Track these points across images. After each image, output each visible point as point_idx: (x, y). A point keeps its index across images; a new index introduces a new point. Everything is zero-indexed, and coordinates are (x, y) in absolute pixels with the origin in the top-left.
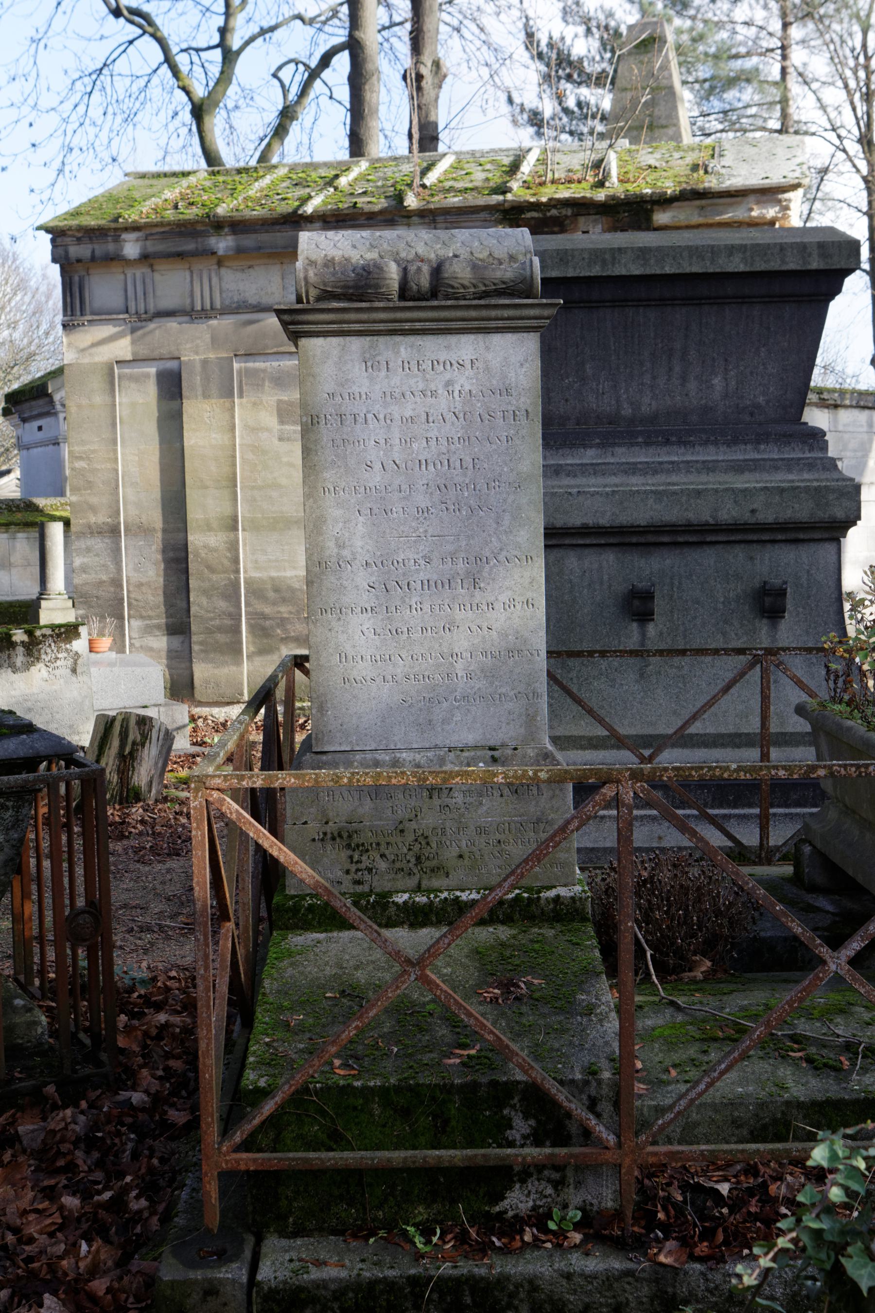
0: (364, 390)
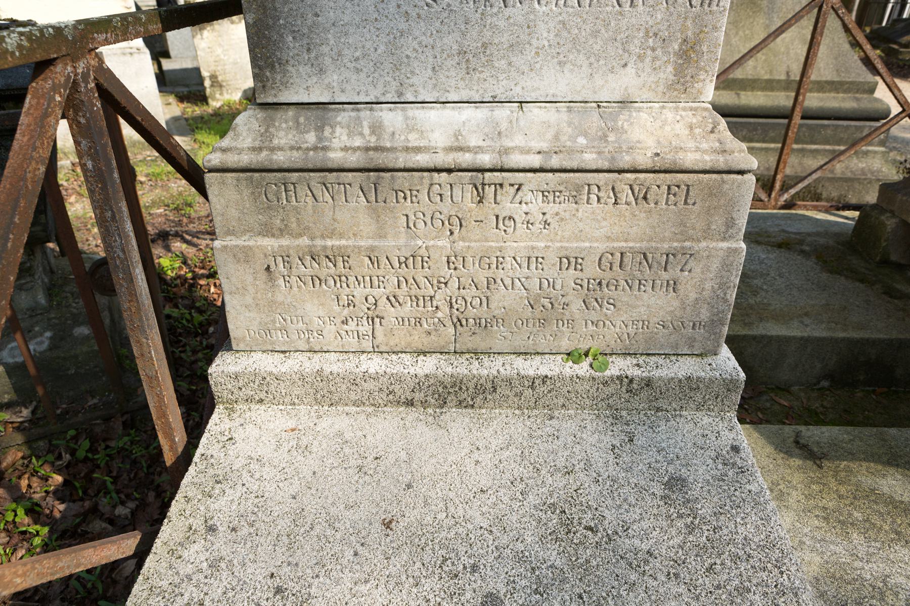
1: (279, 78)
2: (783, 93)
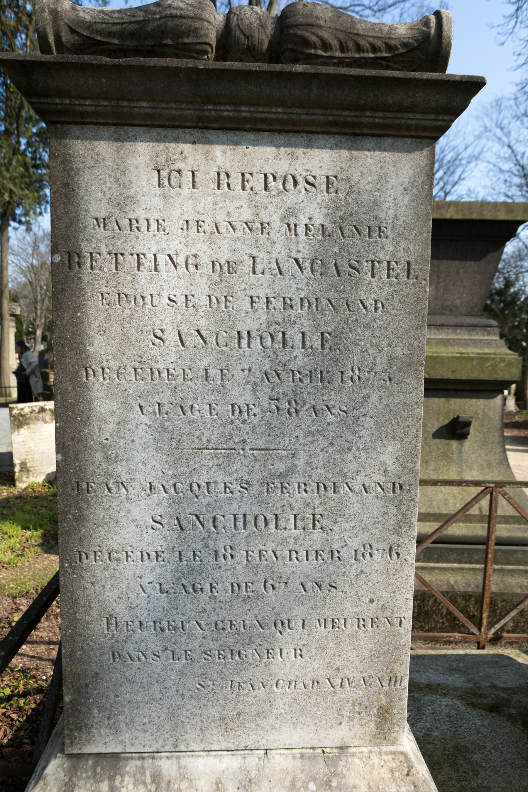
0: (153, 216)
1: (84, 737)
2: (479, 525)
